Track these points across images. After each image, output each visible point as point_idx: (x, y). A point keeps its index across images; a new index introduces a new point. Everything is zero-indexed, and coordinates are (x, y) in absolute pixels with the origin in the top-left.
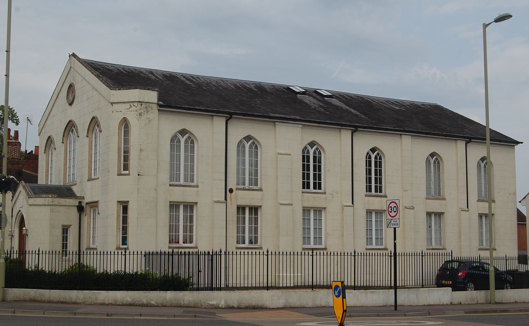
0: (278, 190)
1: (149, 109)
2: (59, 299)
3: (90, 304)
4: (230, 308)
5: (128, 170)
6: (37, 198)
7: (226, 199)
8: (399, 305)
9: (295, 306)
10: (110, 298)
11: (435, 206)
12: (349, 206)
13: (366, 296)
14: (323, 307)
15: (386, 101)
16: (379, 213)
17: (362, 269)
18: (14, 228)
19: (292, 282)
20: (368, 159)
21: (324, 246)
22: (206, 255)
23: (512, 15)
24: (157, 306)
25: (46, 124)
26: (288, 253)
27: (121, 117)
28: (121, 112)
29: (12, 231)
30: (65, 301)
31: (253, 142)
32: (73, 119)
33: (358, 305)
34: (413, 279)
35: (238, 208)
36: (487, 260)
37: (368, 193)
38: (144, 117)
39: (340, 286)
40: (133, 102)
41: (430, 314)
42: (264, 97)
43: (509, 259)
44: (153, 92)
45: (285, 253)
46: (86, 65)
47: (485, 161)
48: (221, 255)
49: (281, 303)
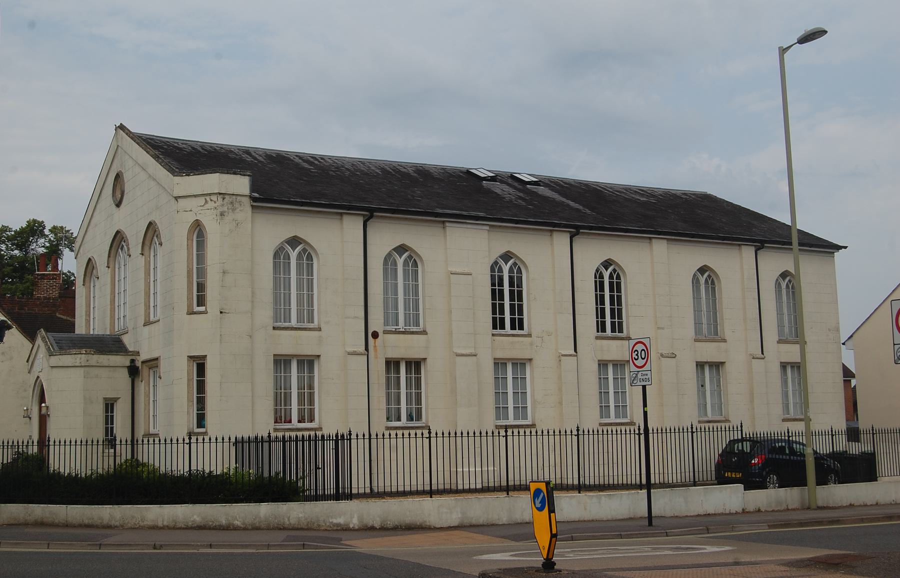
0: (452, 332)
1: (237, 205)
2: (81, 521)
3: (134, 528)
4: (367, 529)
5: (204, 306)
7: (367, 349)
8: (656, 517)
10: (166, 518)
11: (710, 352)
12: (570, 355)
13: (600, 503)
14: (527, 523)
15: (626, 189)
16: (619, 365)
17: (596, 456)
18: (32, 405)
19: (479, 481)
20: (598, 280)
22: (319, 440)
23: (826, 30)
24: (245, 529)
25: (85, 239)
26: (471, 434)
27: (192, 219)
28: (191, 211)
29: (29, 410)
30: (91, 524)
31: (410, 255)
32: (122, 228)
33: (586, 519)
34: (679, 471)
35: (388, 362)
36: (801, 437)
37: (600, 333)
38: (229, 217)
39: (544, 490)
40: (210, 194)
41: (709, 532)
42: (429, 185)
43: (837, 433)
44: (243, 177)
45: (465, 434)
46: (139, 141)
47: (788, 279)
48: (350, 439)
49: (454, 519)
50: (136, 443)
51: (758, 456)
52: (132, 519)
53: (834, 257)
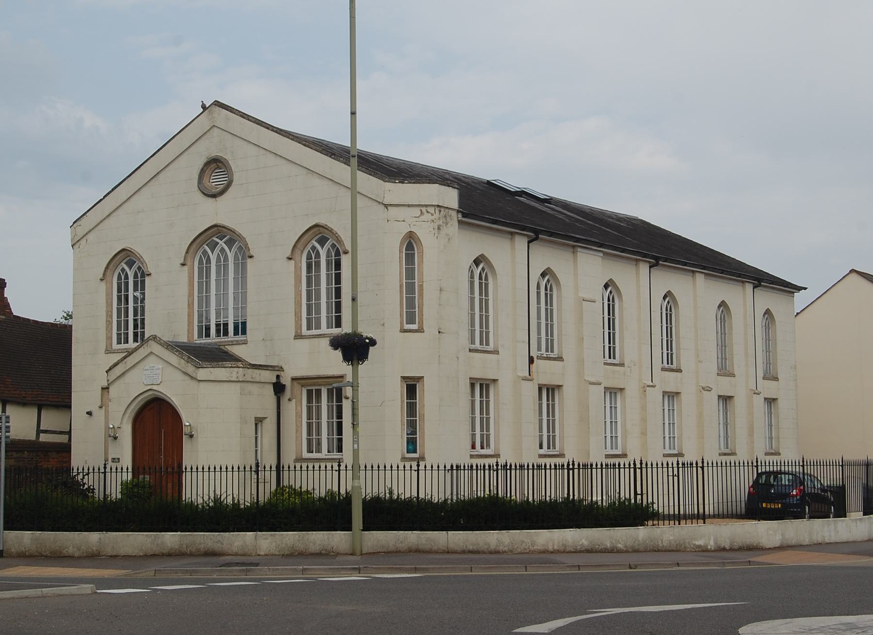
0: (584, 359)
2: (465, 547)
3: (523, 553)
6: (214, 367)
9: (792, 545)
10: (556, 542)
21: (621, 451)
24: (627, 552)
28: (404, 221)
30: (476, 550)
40: (426, 206)
41: (527, 570)
50: (281, 469)
51: (796, 488)
52: (521, 545)
53: (793, 297)
